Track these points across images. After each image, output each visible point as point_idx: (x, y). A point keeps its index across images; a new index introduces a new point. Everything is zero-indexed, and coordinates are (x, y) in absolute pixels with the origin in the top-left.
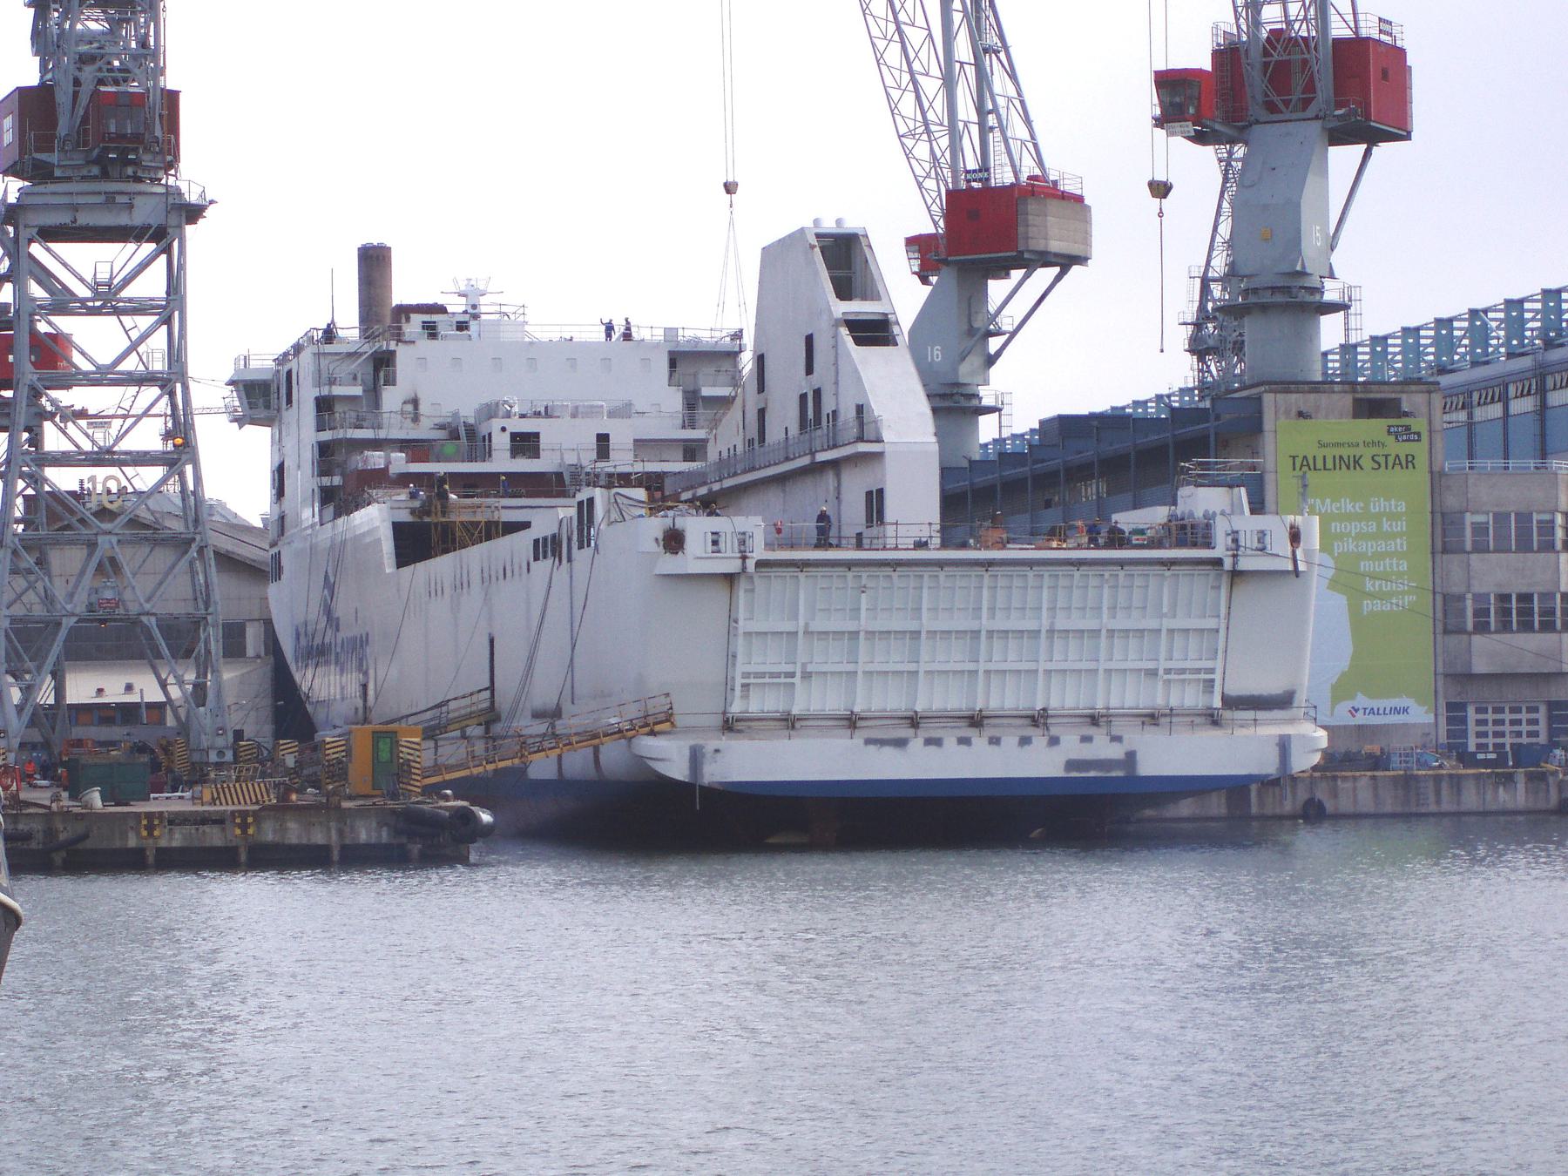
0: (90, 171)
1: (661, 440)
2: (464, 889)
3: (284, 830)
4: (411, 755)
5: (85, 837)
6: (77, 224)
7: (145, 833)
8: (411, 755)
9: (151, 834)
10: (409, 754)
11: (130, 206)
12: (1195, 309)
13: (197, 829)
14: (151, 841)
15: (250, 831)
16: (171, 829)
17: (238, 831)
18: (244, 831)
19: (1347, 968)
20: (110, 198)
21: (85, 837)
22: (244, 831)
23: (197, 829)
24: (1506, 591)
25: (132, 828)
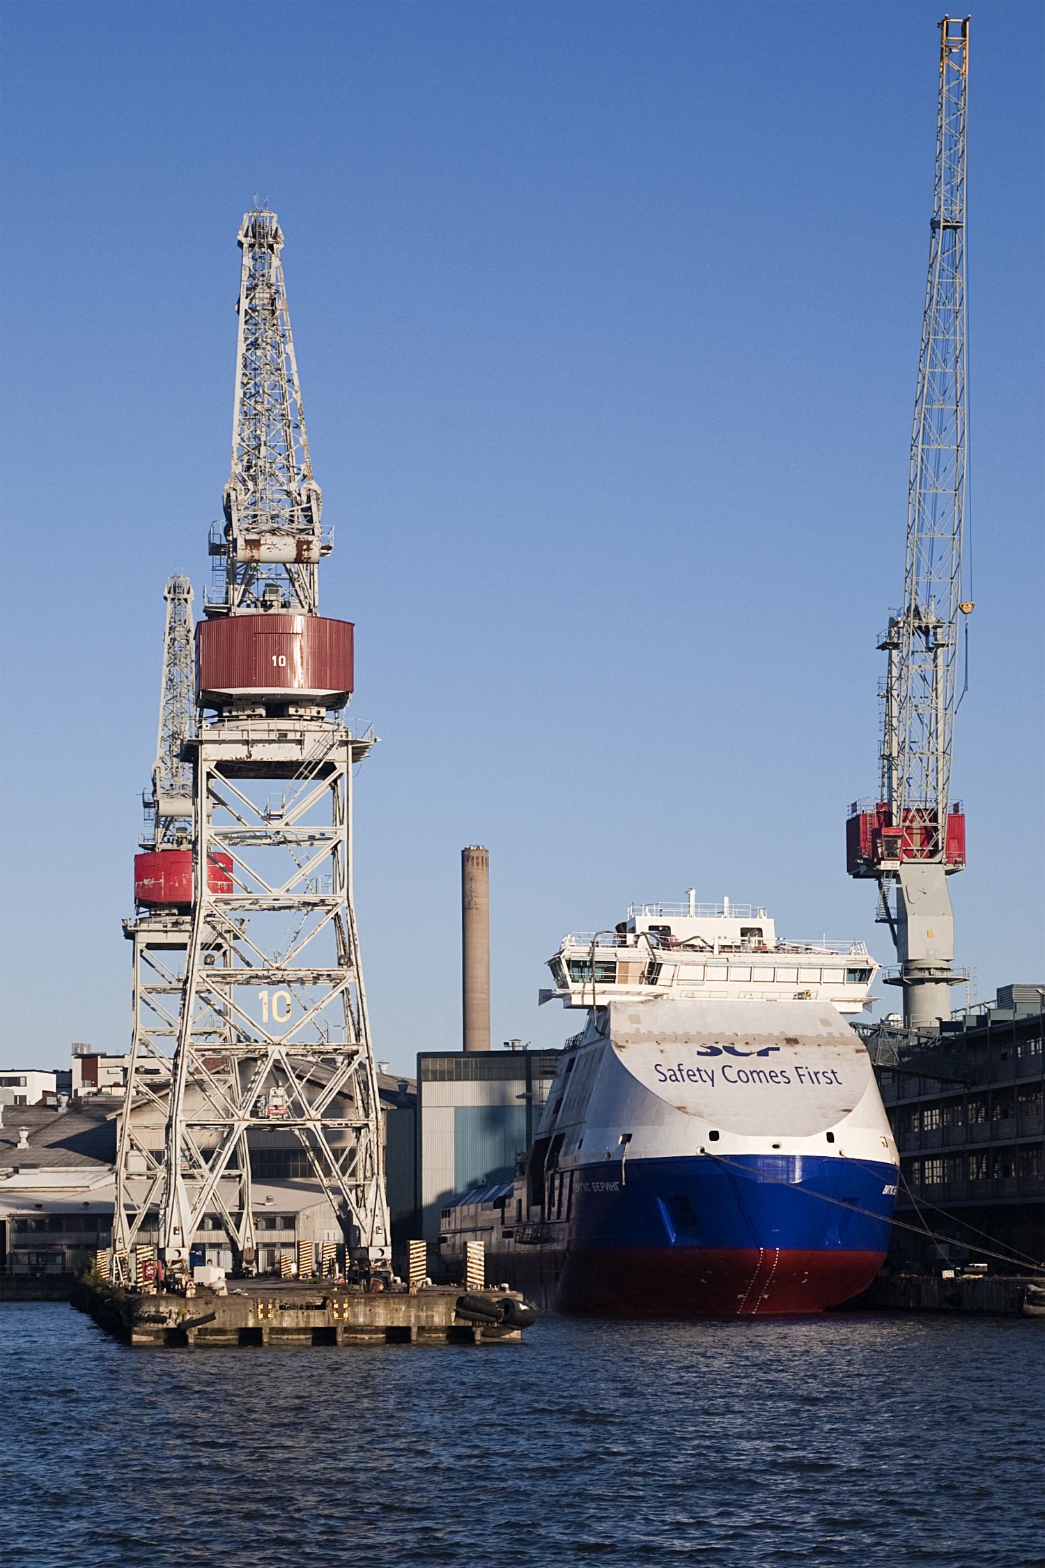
0: (297, 711)
1: (1025, 987)
2: (800, 1392)
3: (373, 1315)
4: (477, 1254)
5: (211, 1317)
6: (252, 759)
7: (261, 1316)
8: (477, 1254)
9: (266, 1317)
10: (474, 1253)
11: (300, 742)
12: (494, 1059)
13: (303, 1313)
14: (265, 1321)
15: (346, 1315)
16: (282, 1313)
17: (336, 1315)
18: (341, 1315)
19: (192, 1379)
20: (283, 738)
21: (211, 1317)
22: (341, 1315)
23: (303, 1313)
24: (301, 1222)
25: (251, 1311)
